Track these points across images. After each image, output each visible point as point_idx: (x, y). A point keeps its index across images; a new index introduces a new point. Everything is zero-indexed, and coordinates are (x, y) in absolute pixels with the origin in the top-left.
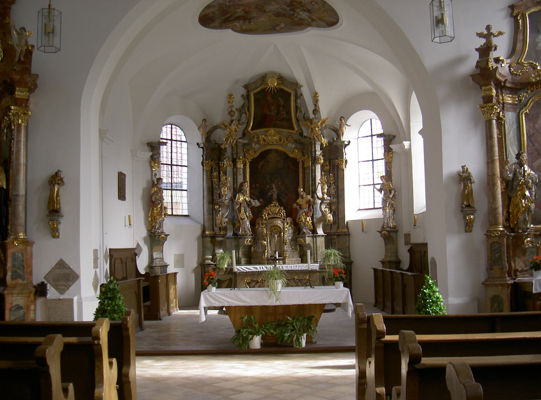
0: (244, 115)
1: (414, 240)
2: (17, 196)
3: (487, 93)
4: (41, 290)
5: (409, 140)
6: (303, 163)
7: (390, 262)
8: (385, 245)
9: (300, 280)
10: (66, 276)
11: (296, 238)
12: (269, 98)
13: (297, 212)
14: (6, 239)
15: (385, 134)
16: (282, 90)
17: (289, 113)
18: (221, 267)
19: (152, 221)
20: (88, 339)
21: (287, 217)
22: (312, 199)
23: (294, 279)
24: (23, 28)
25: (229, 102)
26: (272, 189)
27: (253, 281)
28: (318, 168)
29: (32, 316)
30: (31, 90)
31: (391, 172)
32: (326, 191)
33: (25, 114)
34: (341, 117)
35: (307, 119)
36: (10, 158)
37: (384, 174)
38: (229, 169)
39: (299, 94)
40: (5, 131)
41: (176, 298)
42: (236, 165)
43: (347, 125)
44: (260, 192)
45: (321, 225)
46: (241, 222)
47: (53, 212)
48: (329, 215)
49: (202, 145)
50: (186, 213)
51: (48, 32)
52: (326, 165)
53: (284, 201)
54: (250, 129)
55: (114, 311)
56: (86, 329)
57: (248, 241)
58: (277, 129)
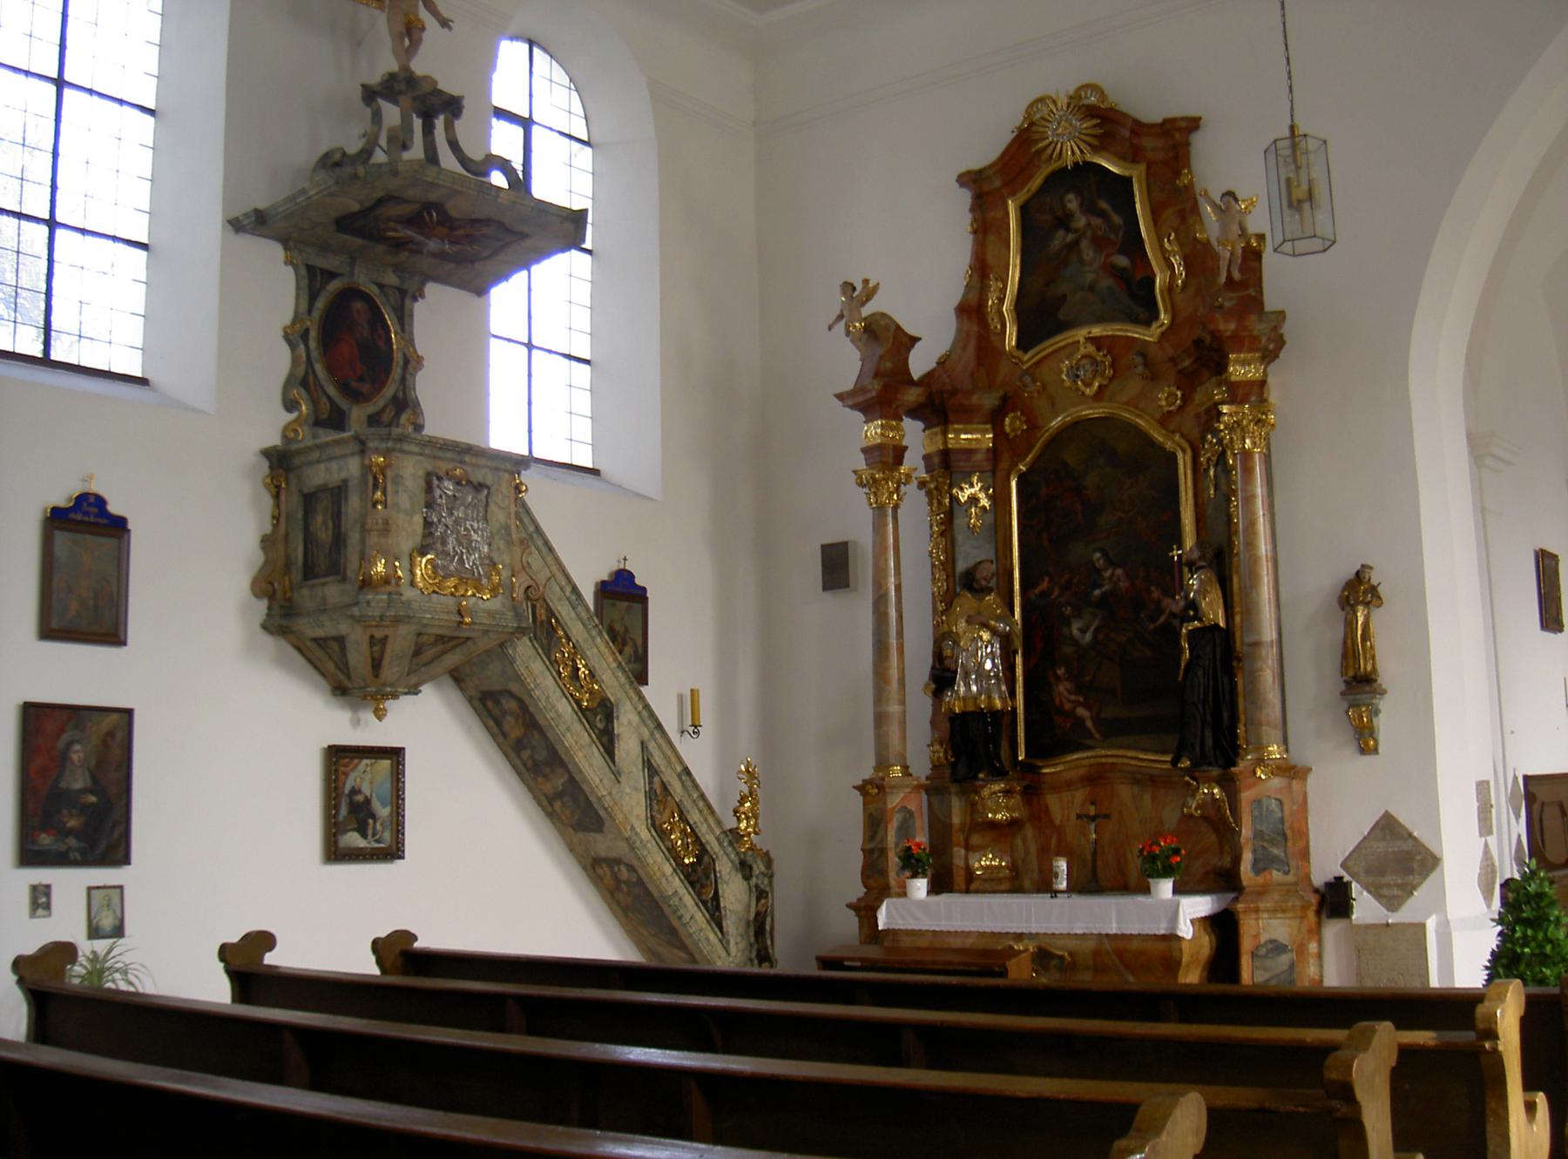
2: (1257, 644)
4: (1335, 900)
10: (1401, 859)
14: (1234, 764)
20: (1464, 1037)
24: (1230, 194)
29: (1312, 970)
30: (1269, 356)
33: (1258, 422)
36: (1230, 543)
40: (1212, 472)
47: (1359, 683)
51: (1298, 199)
55: (1544, 959)
56: (1458, 1009)
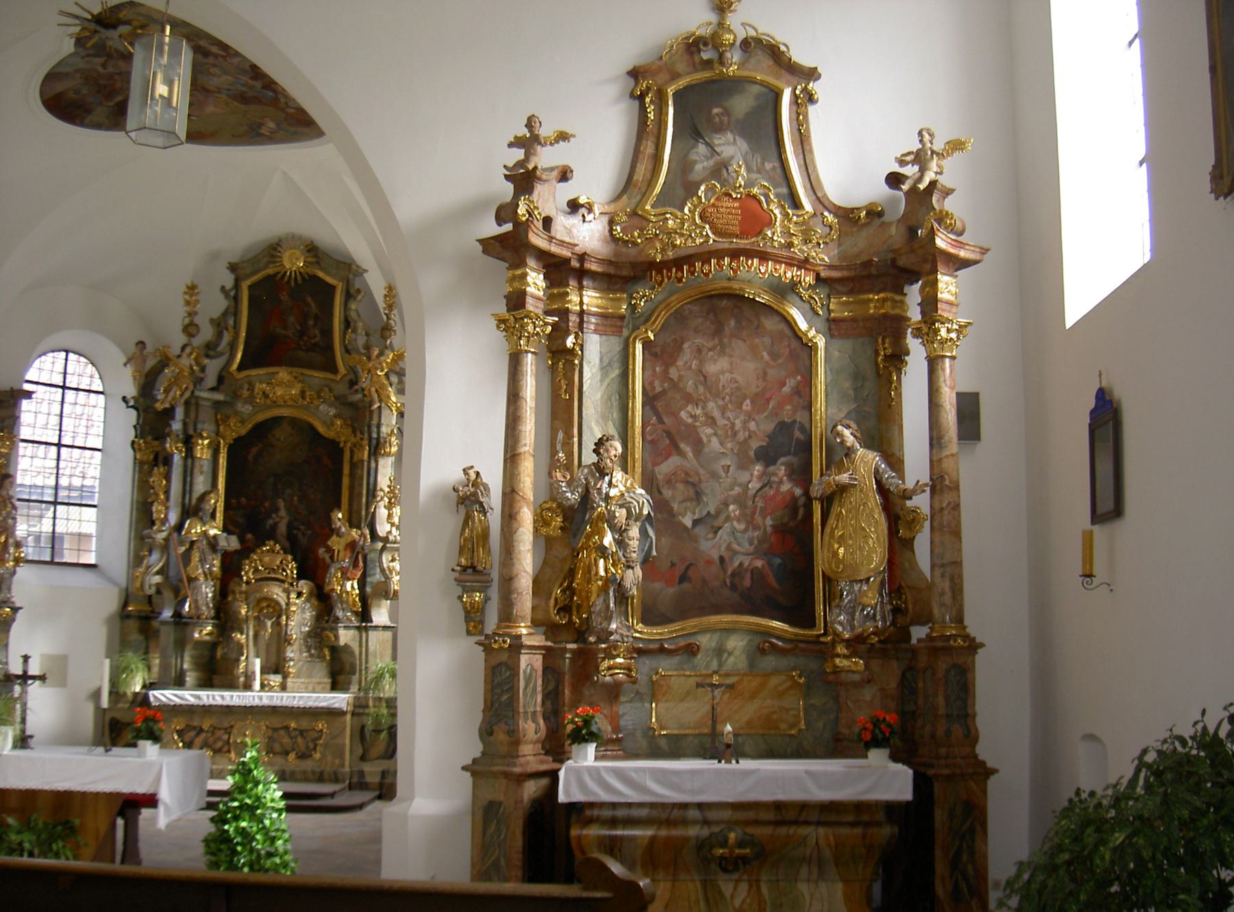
3: (516, 284)
9: (302, 732)
12: (284, 297)
13: (326, 568)
17: (327, 332)
23: (287, 728)
25: (188, 303)
26: (278, 510)
27: (189, 728)
50: (93, 562)
54: (235, 366)
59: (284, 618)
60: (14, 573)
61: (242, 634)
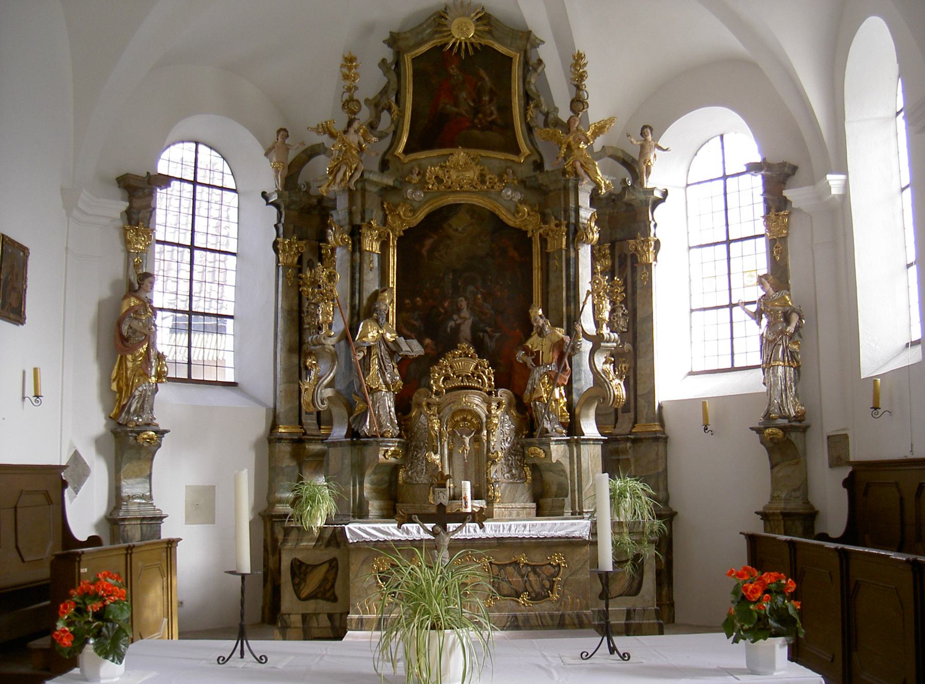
0: (385, 115)
1: (859, 452)
5: (842, 168)
6: (544, 241)
7: (786, 515)
8: (772, 468)
9: (534, 568)
11: (523, 447)
12: (453, 70)
13: (526, 371)
15: (769, 161)
16: (487, 49)
17: (506, 109)
18: (307, 524)
19: (120, 390)
21: (497, 386)
22: (567, 339)
23: (516, 563)
25: (346, 77)
26: (459, 310)
28: (585, 253)
31: (787, 265)
32: (606, 315)
34: (644, 127)
35: (551, 121)
37: (763, 269)
38: (341, 256)
39: (533, 61)
41: (169, 614)
42: (360, 242)
43: (660, 148)
44: (425, 317)
45: (592, 412)
46: (369, 398)
48: (617, 381)
49: (274, 198)
50: (230, 378)
52: (604, 256)
53: (491, 344)
57: (387, 452)
58: (473, 152)
59: (485, 432)
60: (157, 390)
61: (436, 453)
